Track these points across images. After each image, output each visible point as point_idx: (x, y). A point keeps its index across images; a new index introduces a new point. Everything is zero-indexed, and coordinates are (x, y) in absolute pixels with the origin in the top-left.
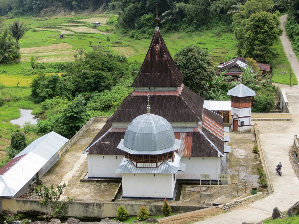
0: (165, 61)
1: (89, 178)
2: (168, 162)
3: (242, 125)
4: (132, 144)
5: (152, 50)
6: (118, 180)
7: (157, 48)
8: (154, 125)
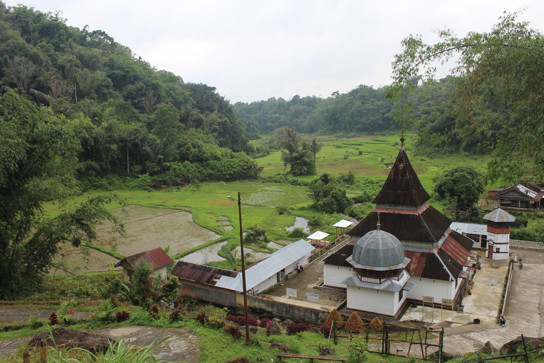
0: (407, 180)
3: (498, 252)
4: (359, 258)
8: (380, 242)
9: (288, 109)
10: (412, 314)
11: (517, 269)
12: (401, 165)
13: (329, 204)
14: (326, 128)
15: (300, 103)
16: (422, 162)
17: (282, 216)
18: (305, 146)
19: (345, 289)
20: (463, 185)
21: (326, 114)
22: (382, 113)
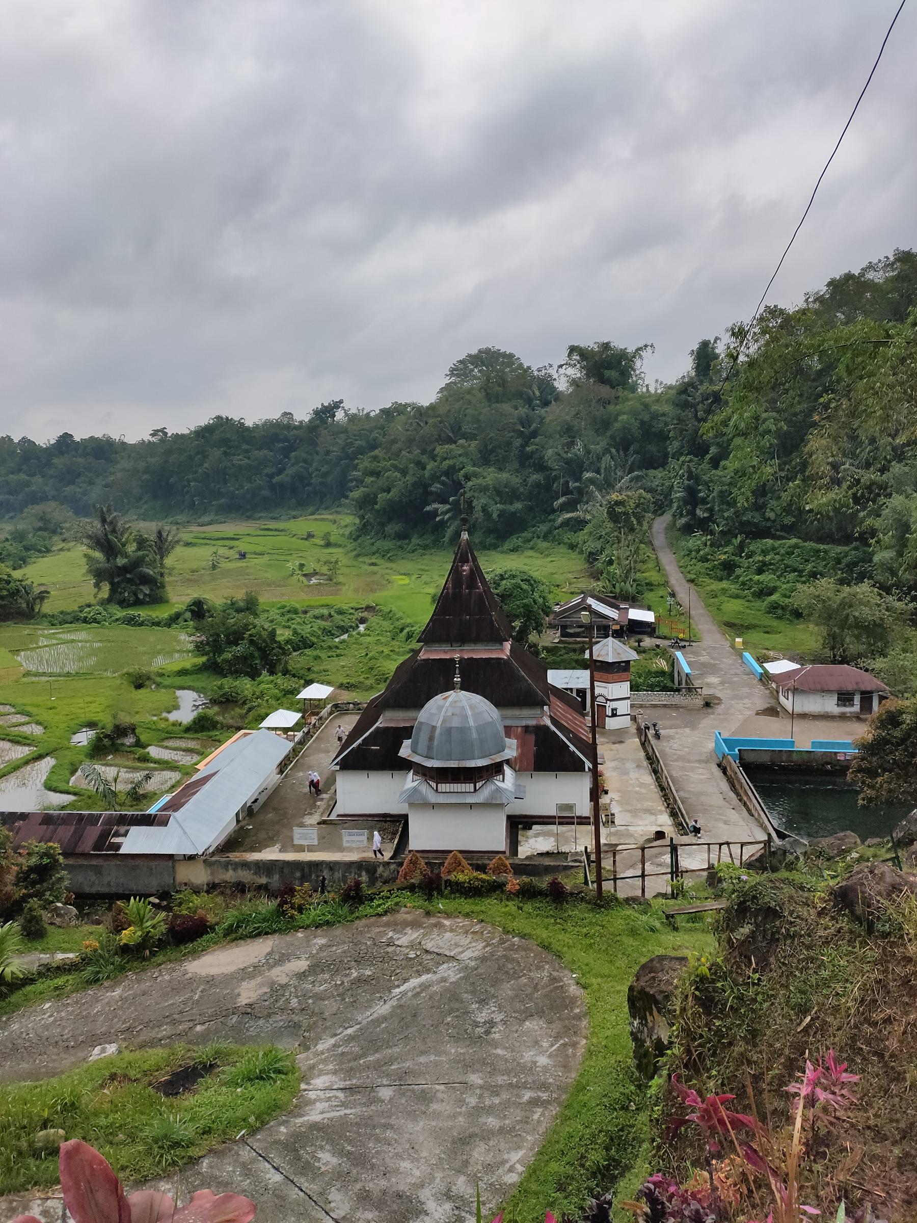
0: (480, 594)
1: (338, 816)
2: (497, 783)
3: (614, 715)
4: (430, 748)
5: (455, 572)
6: (403, 820)
7: (465, 571)
8: (469, 713)
9: (49, 464)
10: (532, 841)
11: (653, 741)
12: (465, 568)
13: (245, 659)
14: (146, 506)
15: (76, 451)
16: (375, 568)
17: (142, 691)
18: (142, 543)
19: (405, 817)
20: (518, 603)
21: (145, 476)
22: (267, 475)
